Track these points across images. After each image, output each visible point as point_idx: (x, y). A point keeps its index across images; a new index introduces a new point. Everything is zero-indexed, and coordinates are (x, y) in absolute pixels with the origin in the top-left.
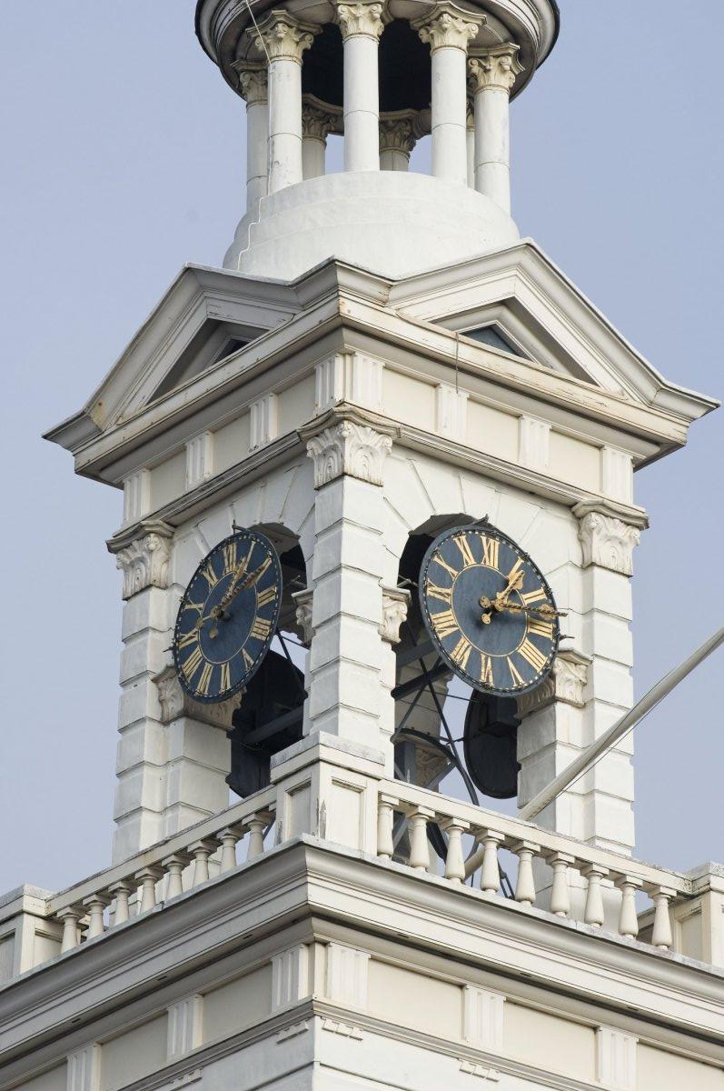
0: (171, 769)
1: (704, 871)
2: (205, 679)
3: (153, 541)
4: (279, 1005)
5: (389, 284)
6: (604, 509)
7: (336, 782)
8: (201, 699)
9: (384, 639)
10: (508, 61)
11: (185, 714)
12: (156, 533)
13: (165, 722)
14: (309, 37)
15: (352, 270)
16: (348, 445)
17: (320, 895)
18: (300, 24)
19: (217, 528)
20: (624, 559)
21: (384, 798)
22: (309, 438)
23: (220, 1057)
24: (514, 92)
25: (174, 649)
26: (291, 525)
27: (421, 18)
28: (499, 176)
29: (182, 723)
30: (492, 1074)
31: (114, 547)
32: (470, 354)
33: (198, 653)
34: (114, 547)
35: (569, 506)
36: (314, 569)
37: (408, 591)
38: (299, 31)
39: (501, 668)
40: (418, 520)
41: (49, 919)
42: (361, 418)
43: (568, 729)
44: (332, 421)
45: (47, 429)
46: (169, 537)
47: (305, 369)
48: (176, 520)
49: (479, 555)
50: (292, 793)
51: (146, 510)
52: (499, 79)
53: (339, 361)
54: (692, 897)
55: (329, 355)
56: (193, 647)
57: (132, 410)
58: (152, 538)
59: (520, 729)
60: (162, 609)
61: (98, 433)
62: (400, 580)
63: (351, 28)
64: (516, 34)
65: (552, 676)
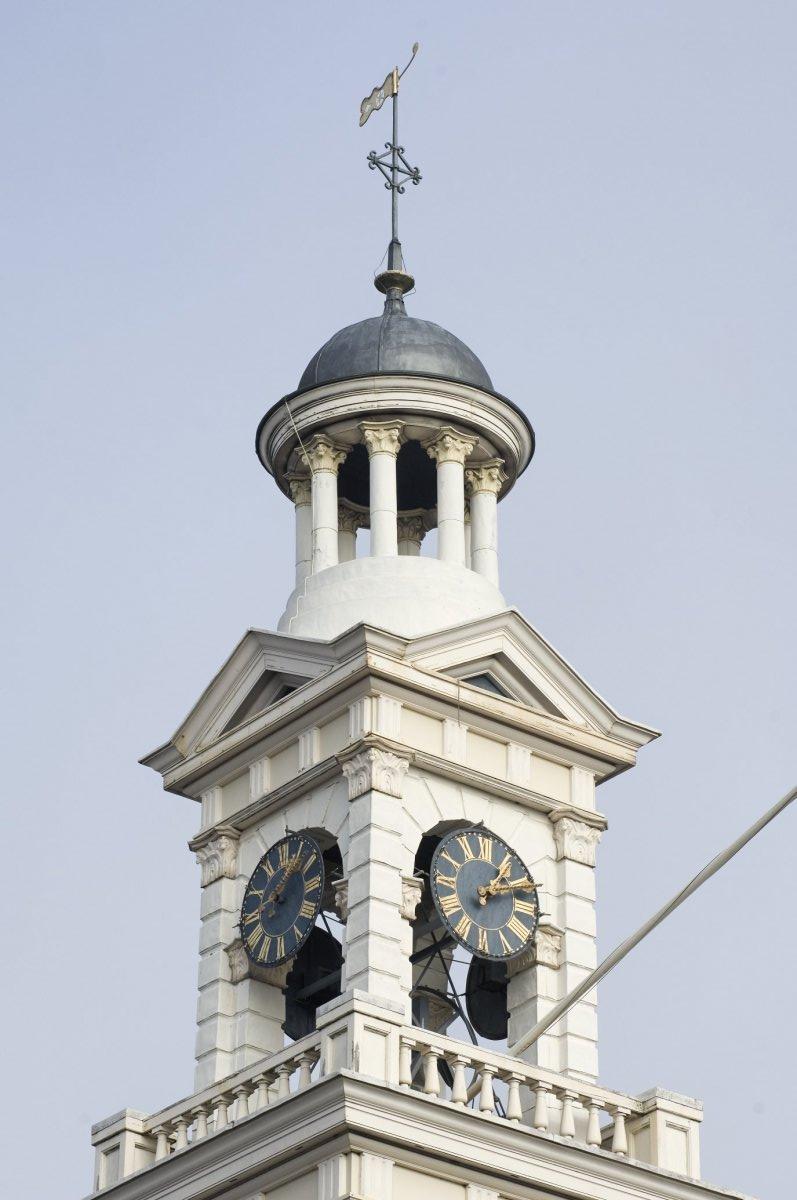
3: (224, 842)
5: (406, 642)
6: (574, 815)
7: (367, 1028)
8: (262, 964)
9: (404, 917)
10: (496, 472)
11: (250, 976)
13: (234, 983)
14: (342, 455)
17: (355, 1116)
18: (336, 445)
19: (273, 832)
21: (404, 1040)
24: (501, 496)
26: (331, 829)
27: (429, 439)
29: (247, 982)
33: (259, 928)
35: (546, 813)
36: (349, 863)
37: (422, 880)
38: (335, 450)
39: (494, 940)
40: (429, 824)
41: (146, 1135)
42: (384, 746)
43: (545, 983)
44: (362, 748)
46: (236, 839)
48: (242, 826)
49: (476, 851)
51: (219, 818)
52: (489, 486)
54: (642, 1115)
56: (255, 924)
59: (509, 986)
60: (231, 894)
61: (182, 758)
62: (415, 871)
63: (375, 447)
64: (502, 451)
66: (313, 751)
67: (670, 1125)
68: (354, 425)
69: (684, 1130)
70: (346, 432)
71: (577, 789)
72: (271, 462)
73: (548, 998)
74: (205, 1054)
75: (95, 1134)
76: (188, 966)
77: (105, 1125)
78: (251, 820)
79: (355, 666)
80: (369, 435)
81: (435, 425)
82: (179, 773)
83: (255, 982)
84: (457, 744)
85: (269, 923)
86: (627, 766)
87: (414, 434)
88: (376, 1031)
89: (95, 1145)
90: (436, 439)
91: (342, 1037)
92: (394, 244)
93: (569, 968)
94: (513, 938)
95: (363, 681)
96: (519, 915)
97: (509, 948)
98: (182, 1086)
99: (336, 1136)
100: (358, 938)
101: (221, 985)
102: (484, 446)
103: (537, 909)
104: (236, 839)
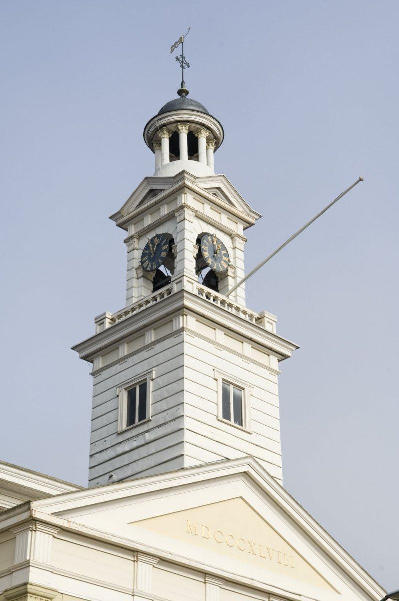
0: (140, 289)
1: (263, 313)
2: (149, 267)
3: (135, 239)
4: (175, 329)
5: (195, 178)
6: (238, 235)
7: (187, 281)
8: (148, 271)
10: (214, 144)
11: (143, 276)
12: (136, 238)
13: (138, 279)
15: (188, 173)
16: (186, 213)
18: (169, 131)
19: (152, 235)
20: (242, 248)
22: (176, 212)
23: (159, 343)
24: (215, 151)
25: (141, 262)
26: (170, 232)
27: (196, 131)
28: (212, 166)
29: (142, 278)
30: (221, 349)
31: (125, 242)
32: (212, 197)
33: (147, 261)
34: (125, 242)
35: (230, 235)
38: (169, 133)
39: (218, 266)
40: (200, 232)
41: (112, 319)
42: (189, 207)
43: (231, 282)
44: (182, 207)
45: (72, 346)
46: (139, 239)
47: (175, 198)
48: (140, 235)
50: (176, 284)
51: (133, 233)
52: (212, 148)
53: (183, 195)
54: (259, 319)
55: (181, 194)
56: (146, 260)
57: (130, 211)
58: (135, 239)
59: (219, 283)
60: (138, 254)
61: (122, 216)
63: (181, 131)
64: (216, 137)
65: (227, 270)
66: (165, 211)
67: (268, 322)
68: (174, 125)
69: (272, 324)
70: (172, 127)
71: (238, 228)
72: (147, 136)
73: (231, 286)
74: (128, 299)
75: (95, 319)
76: (124, 275)
77: (99, 317)
78: (145, 232)
79: (180, 184)
80: (180, 127)
81: (198, 126)
82: (121, 221)
83: (145, 279)
84: (207, 210)
85: (151, 260)
86: (253, 224)
87: (192, 129)
88: (190, 282)
89: (95, 323)
90: (198, 131)
91: (180, 283)
92: (183, 82)
93: (237, 278)
94: (223, 267)
95: (183, 188)
96: (224, 261)
97: (221, 269)
98: (121, 305)
99: (179, 310)
100: (181, 260)
101: (134, 279)
102: (211, 135)
103: (229, 260)
104: (139, 239)
